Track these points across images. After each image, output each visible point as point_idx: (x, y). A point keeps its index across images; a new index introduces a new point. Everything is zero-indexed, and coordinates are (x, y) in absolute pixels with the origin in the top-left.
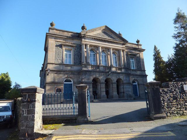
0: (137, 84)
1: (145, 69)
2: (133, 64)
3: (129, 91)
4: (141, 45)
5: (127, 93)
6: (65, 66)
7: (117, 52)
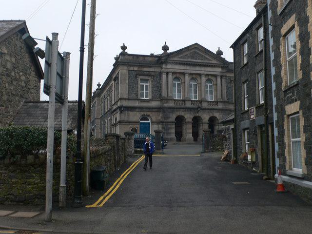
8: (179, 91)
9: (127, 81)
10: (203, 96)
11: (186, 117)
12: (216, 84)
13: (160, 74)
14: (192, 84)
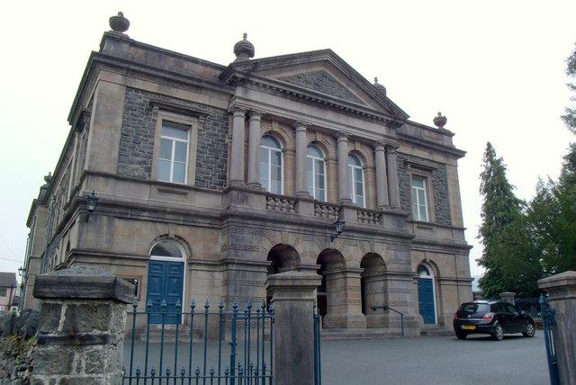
0: (432, 276)
2: (422, 202)
3: (405, 304)
4: (450, 135)
5: (400, 309)
6: (160, 191)
7: (366, 152)
9: (119, 121)
11: (300, 249)
13: (229, 114)
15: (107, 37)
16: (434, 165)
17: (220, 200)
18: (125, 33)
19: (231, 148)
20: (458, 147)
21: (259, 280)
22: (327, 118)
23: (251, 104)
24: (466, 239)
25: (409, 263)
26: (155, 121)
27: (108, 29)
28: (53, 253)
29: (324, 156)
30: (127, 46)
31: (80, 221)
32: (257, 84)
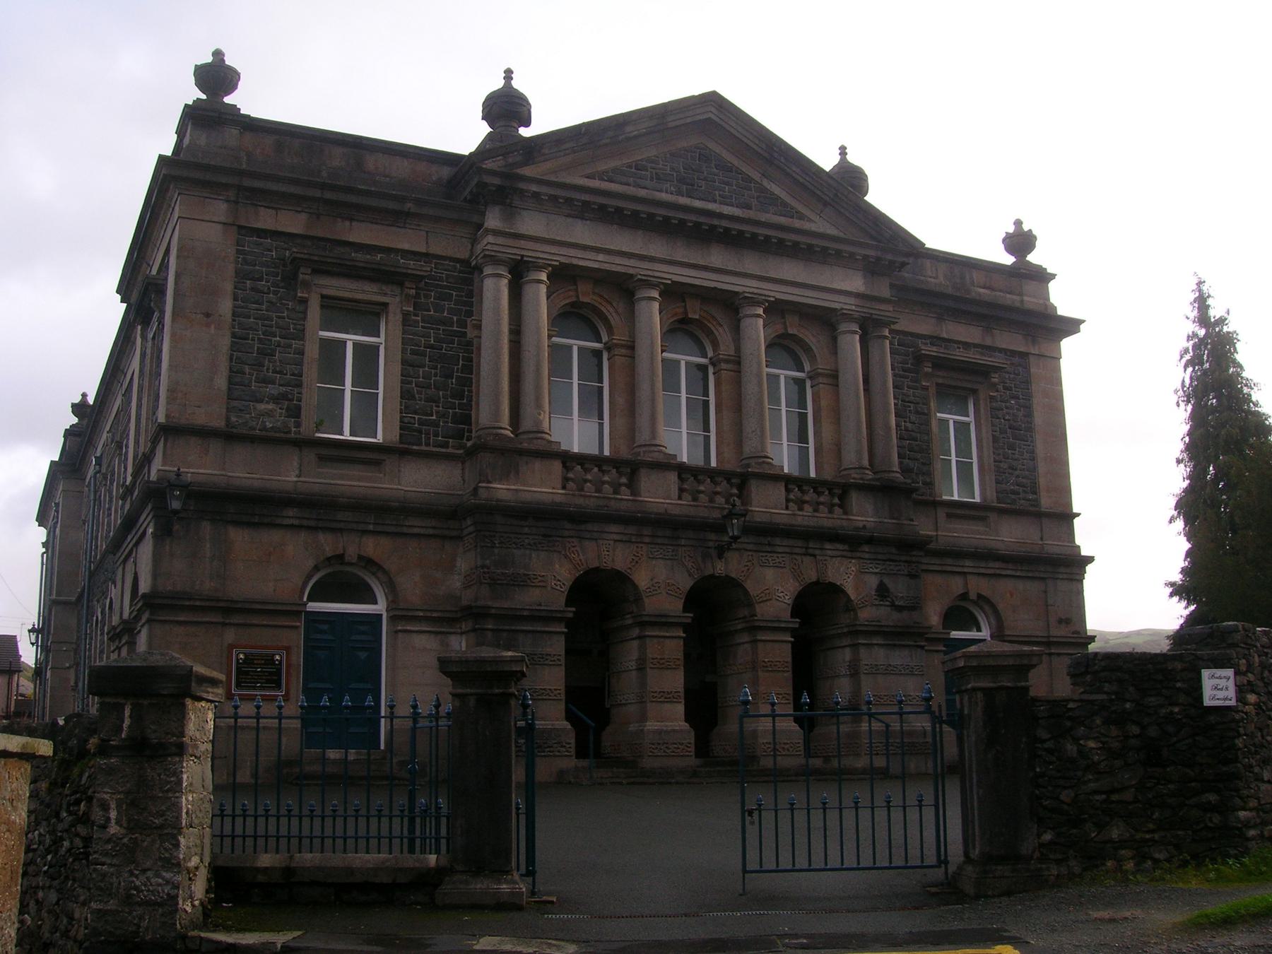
1: (1069, 504)
2: (963, 450)
6: (321, 458)
8: (592, 403)
9: (226, 307)
10: (748, 449)
11: (642, 579)
12: (834, 376)
13: (469, 273)
14: (678, 362)
15: (193, 117)
16: (997, 360)
17: (457, 472)
18: (228, 100)
19: (479, 349)
20: (1062, 311)
21: (549, 650)
22: (836, 286)
23: (523, 243)
24: (1078, 541)
25: (915, 606)
26: (304, 301)
27: (194, 94)
28: (105, 593)
29: (710, 354)
30: (235, 132)
31: (154, 535)
32: (536, 195)
